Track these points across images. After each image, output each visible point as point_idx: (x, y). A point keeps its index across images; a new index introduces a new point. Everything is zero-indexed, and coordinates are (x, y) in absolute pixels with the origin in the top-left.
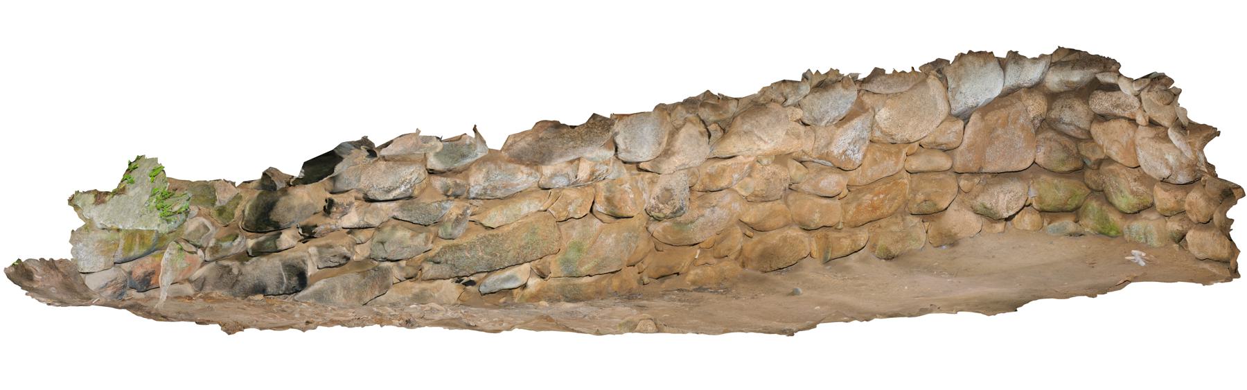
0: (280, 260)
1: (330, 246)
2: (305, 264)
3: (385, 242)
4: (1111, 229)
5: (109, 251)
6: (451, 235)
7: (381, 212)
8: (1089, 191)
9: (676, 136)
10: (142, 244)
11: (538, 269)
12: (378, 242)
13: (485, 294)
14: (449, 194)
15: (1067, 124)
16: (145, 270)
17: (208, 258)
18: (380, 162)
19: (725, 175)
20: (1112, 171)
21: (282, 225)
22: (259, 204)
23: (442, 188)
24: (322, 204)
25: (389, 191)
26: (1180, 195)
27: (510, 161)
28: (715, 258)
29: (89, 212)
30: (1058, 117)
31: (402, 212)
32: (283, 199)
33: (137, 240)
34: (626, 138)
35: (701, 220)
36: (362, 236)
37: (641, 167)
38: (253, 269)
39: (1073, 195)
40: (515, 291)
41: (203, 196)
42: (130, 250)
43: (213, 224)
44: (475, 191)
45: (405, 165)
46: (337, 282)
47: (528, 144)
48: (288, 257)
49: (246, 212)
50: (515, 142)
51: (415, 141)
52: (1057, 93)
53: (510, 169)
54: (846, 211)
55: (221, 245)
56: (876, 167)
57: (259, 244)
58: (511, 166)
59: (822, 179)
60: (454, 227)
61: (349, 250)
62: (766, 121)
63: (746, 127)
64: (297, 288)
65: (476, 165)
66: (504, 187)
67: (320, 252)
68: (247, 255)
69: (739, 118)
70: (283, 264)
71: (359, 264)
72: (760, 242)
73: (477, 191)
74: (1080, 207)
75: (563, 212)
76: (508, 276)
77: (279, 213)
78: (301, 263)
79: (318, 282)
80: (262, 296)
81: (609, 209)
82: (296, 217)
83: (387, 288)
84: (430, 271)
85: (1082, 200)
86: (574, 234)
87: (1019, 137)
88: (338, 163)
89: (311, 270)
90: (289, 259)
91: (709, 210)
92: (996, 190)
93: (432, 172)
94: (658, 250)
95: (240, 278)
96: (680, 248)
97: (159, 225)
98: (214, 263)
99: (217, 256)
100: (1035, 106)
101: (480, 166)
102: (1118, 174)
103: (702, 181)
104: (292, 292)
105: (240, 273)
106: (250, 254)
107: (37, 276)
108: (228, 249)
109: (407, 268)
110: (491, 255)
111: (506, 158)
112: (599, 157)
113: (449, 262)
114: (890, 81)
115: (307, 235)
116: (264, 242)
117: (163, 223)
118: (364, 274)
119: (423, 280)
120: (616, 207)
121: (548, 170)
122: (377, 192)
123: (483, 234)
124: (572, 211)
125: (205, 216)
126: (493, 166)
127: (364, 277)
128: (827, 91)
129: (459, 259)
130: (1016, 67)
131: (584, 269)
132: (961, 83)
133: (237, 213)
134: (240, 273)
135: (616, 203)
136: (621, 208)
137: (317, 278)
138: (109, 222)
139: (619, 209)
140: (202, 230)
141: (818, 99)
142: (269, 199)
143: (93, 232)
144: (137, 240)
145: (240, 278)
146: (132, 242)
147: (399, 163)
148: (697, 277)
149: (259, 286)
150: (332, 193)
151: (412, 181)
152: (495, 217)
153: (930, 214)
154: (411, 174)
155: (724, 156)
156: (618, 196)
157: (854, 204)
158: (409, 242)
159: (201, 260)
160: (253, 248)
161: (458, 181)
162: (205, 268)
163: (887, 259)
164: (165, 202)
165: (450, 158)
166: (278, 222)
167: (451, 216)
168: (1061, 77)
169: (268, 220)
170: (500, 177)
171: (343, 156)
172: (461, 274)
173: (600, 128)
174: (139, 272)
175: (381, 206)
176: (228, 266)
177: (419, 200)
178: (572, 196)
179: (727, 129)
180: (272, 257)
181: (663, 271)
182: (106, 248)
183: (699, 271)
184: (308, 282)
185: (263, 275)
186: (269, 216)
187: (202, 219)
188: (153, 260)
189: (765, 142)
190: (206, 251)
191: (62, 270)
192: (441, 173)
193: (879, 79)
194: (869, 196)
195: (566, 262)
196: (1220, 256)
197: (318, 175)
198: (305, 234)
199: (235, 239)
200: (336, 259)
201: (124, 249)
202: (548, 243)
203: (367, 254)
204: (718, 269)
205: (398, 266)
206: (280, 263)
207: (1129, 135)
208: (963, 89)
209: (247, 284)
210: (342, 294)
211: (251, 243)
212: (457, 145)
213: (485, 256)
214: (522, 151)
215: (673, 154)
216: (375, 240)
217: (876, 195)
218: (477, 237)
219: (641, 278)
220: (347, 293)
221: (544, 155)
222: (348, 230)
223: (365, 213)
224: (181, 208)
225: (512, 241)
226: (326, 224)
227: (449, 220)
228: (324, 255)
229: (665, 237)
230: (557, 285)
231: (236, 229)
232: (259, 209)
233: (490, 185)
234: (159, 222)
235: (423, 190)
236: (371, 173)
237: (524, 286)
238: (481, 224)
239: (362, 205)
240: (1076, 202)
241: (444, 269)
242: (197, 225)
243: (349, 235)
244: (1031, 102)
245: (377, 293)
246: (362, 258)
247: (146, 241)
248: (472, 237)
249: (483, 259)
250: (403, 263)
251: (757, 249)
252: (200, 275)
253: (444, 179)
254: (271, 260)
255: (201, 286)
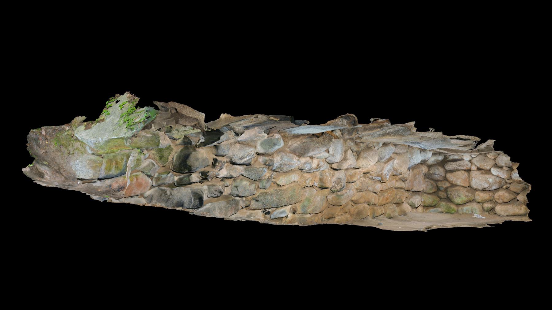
0: (191, 190)
1: (214, 185)
2: (202, 193)
3: (238, 187)
4: (452, 211)
5: (96, 167)
6: (265, 186)
7: (237, 170)
8: (439, 199)
9: (347, 153)
10: (117, 168)
11: (293, 209)
12: (234, 186)
13: (272, 219)
14: (267, 164)
15: (437, 175)
16: (119, 185)
17: (154, 184)
18: (237, 144)
19: (356, 175)
20: (455, 190)
21: (193, 169)
22: (181, 155)
23: (263, 161)
24: (211, 161)
25: (242, 159)
26: (491, 194)
27: (290, 153)
28: (343, 213)
29: (81, 134)
30: (433, 172)
31: (246, 172)
32: (194, 153)
33: (114, 164)
34: (333, 149)
35: (346, 194)
36: (228, 182)
37: (332, 166)
38: (177, 193)
39: (434, 201)
40: (284, 218)
41: (152, 141)
42: (110, 170)
43: (157, 163)
44: (276, 165)
45: (248, 147)
46: (216, 205)
47: (298, 145)
48: (194, 188)
49: (174, 160)
50: (292, 144)
51: (255, 133)
52: (430, 165)
53: (291, 156)
54: (379, 200)
55: (161, 176)
56: (390, 183)
57: (180, 179)
58: (291, 155)
59: (376, 185)
60: (266, 183)
61: (222, 188)
62: (372, 154)
63: (365, 155)
64: (198, 205)
65: (276, 154)
66: (289, 164)
67: (209, 188)
68: (174, 185)
69: (362, 152)
70: (192, 192)
71: (226, 197)
72: (356, 208)
73: (277, 166)
74: (436, 205)
75: (304, 183)
76: (282, 211)
77: (191, 161)
78: (201, 192)
79: (207, 204)
80: (182, 208)
81: (320, 184)
82: (200, 165)
83: (238, 210)
84: (254, 204)
85: (437, 202)
86: (307, 194)
87: (421, 179)
88: (222, 135)
89: (205, 198)
90: (195, 189)
91: (348, 190)
92: (414, 197)
93: (258, 154)
94: (328, 207)
95: (171, 197)
96: (336, 207)
97: (125, 133)
98: (157, 187)
99: (159, 183)
100: (424, 169)
101: (278, 154)
102: (459, 190)
103: (347, 178)
104: (196, 208)
105: (171, 194)
106: (176, 185)
107: (46, 176)
108: (165, 179)
109: (246, 201)
110: (278, 200)
111: (288, 151)
112: (324, 156)
113: (262, 201)
114: (402, 147)
115: (204, 177)
116: (183, 178)
117: (128, 131)
118: (228, 202)
119: (250, 209)
120: (324, 182)
121: (303, 160)
122: (236, 159)
123: (276, 189)
124: (307, 183)
125: (152, 159)
126: (284, 154)
127: (228, 204)
128: (387, 146)
129: (266, 200)
130: (424, 153)
131: (309, 210)
132: (413, 155)
133: (170, 159)
134: (171, 194)
135: (324, 181)
136: (326, 183)
137: (208, 202)
138: (93, 137)
139: (325, 184)
140: (151, 166)
141: (384, 149)
142: (186, 153)
143: (86, 155)
144: (114, 164)
145: (171, 197)
146: (111, 165)
147: (245, 145)
148: (339, 220)
149: (180, 202)
150: (216, 156)
151: (252, 155)
152: (282, 180)
153: (399, 204)
154: (251, 152)
155: (356, 167)
156: (325, 178)
157: (382, 197)
158: (248, 188)
159: (150, 185)
160: (177, 181)
161: (271, 158)
162: (152, 190)
163: (389, 218)
164: (129, 116)
165: (268, 145)
166: (191, 166)
167: (266, 177)
168: (435, 158)
169: (186, 165)
170: (287, 159)
171: (224, 132)
172: (266, 207)
173: (328, 140)
174: (115, 186)
175: (237, 167)
176: (164, 190)
177: (254, 166)
178: (307, 176)
179: (359, 155)
180: (187, 188)
181: (330, 216)
182: (94, 165)
183: (339, 217)
184: (204, 203)
185: (182, 196)
186: (186, 162)
187: (151, 160)
188: (123, 180)
189: (372, 162)
190: (153, 180)
191: (65, 175)
192: (262, 155)
193: (398, 146)
194: (386, 194)
195: (304, 206)
196: (518, 213)
197: (212, 141)
198: (203, 177)
199: (169, 173)
200: (216, 193)
201: (106, 169)
202: (298, 196)
203: (229, 192)
204: (345, 217)
205: (242, 200)
206: (191, 191)
207: (465, 175)
208: (414, 157)
209: (174, 200)
210: (218, 211)
211: (176, 178)
212: (271, 139)
213: (276, 200)
214: (296, 148)
215: (348, 159)
216: (233, 185)
217: (388, 194)
218: (274, 189)
219: (322, 218)
220: (221, 211)
221: (306, 150)
222: (221, 179)
223: (230, 170)
224: (141, 120)
225: (286, 194)
226: (213, 171)
227: (265, 179)
228: (211, 190)
229: (332, 202)
230: (298, 218)
231: (169, 169)
232: (181, 158)
233: (283, 162)
234: (125, 131)
235: (255, 162)
236: (233, 149)
237: (287, 217)
238: (276, 183)
239: (228, 166)
240: (435, 203)
241: (259, 204)
242: (148, 163)
243: (222, 182)
244: (423, 168)
245: (233, 213)
246: (227, 194)
247: (119, 166)
248: (272, 190)
249: (275, 201)
250: (244, 199)
251: (356, 211)
252: (150, 193)
253: (264, 157)
254: (186, 189)
255: (150, 200)
